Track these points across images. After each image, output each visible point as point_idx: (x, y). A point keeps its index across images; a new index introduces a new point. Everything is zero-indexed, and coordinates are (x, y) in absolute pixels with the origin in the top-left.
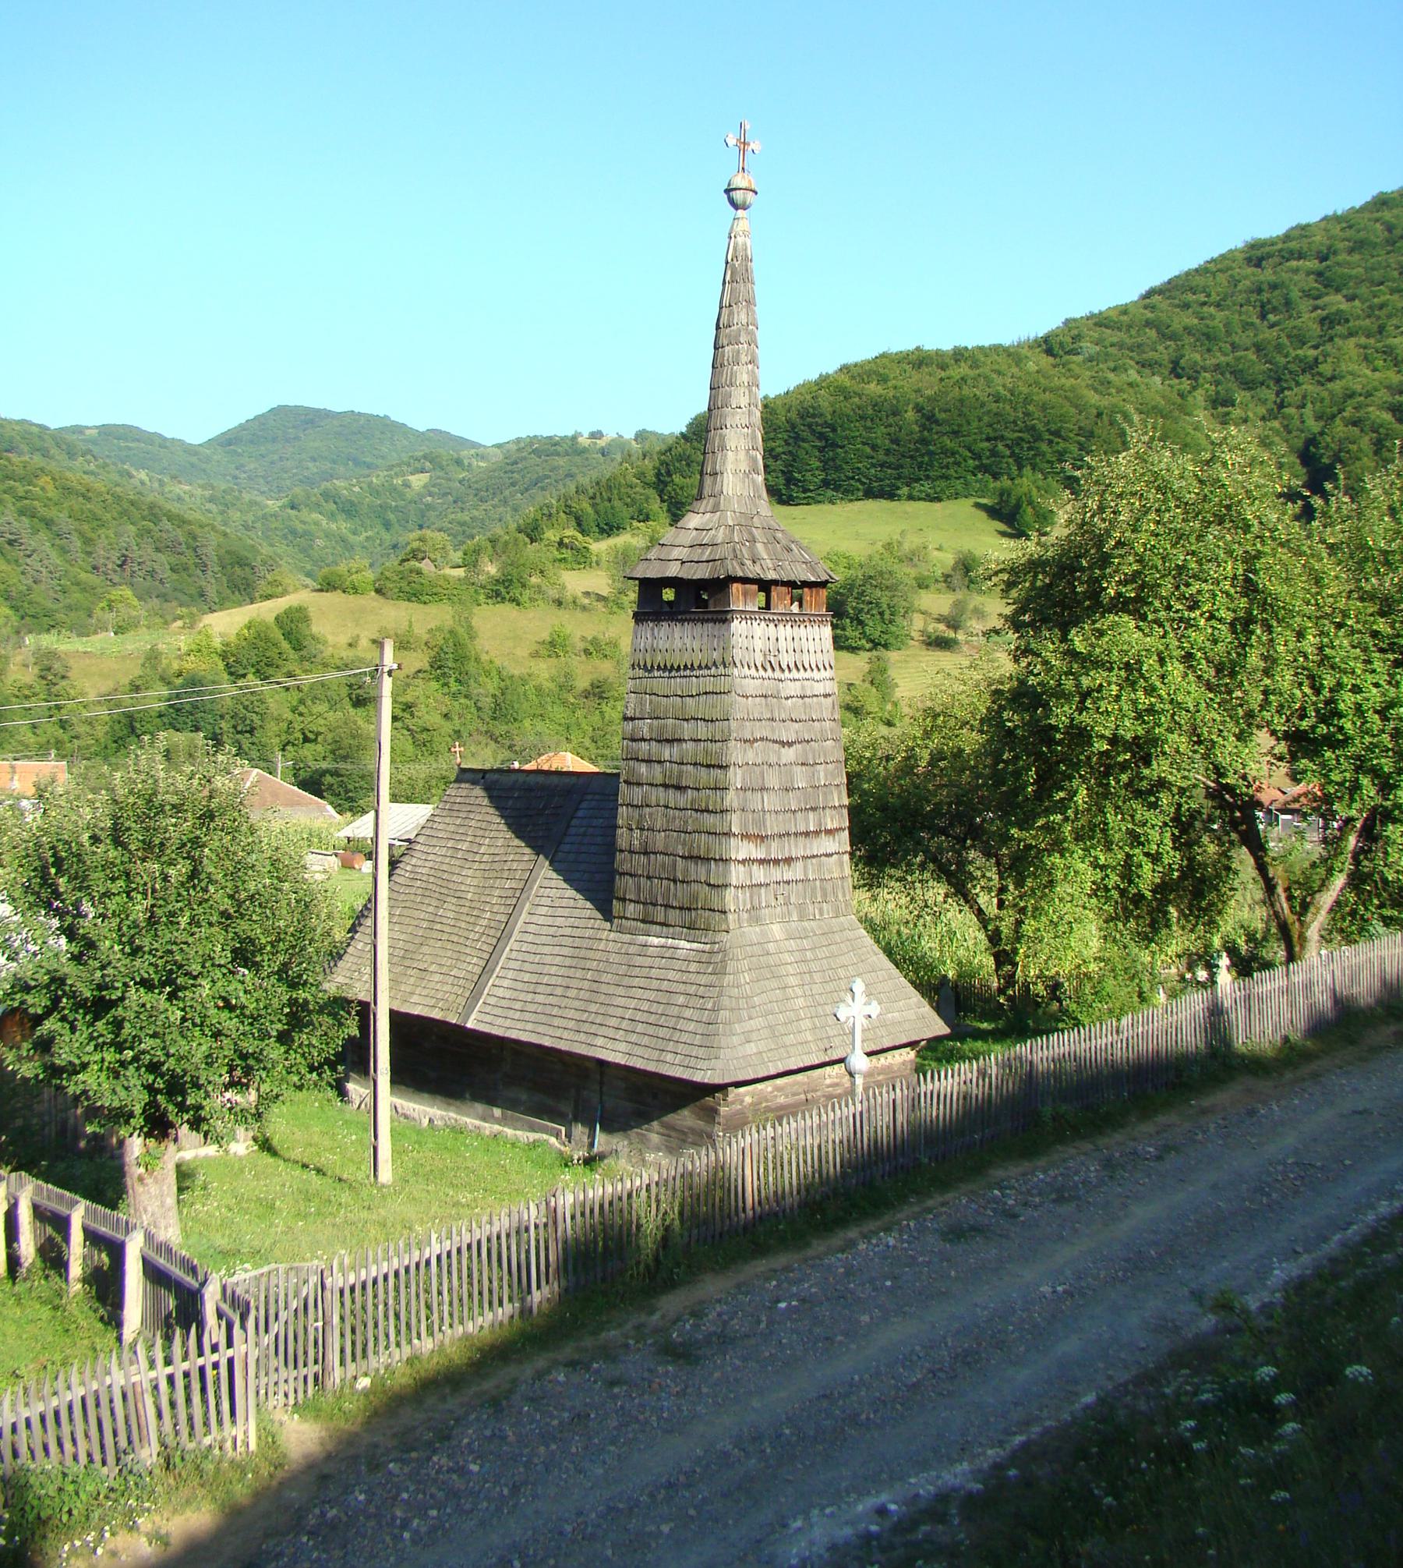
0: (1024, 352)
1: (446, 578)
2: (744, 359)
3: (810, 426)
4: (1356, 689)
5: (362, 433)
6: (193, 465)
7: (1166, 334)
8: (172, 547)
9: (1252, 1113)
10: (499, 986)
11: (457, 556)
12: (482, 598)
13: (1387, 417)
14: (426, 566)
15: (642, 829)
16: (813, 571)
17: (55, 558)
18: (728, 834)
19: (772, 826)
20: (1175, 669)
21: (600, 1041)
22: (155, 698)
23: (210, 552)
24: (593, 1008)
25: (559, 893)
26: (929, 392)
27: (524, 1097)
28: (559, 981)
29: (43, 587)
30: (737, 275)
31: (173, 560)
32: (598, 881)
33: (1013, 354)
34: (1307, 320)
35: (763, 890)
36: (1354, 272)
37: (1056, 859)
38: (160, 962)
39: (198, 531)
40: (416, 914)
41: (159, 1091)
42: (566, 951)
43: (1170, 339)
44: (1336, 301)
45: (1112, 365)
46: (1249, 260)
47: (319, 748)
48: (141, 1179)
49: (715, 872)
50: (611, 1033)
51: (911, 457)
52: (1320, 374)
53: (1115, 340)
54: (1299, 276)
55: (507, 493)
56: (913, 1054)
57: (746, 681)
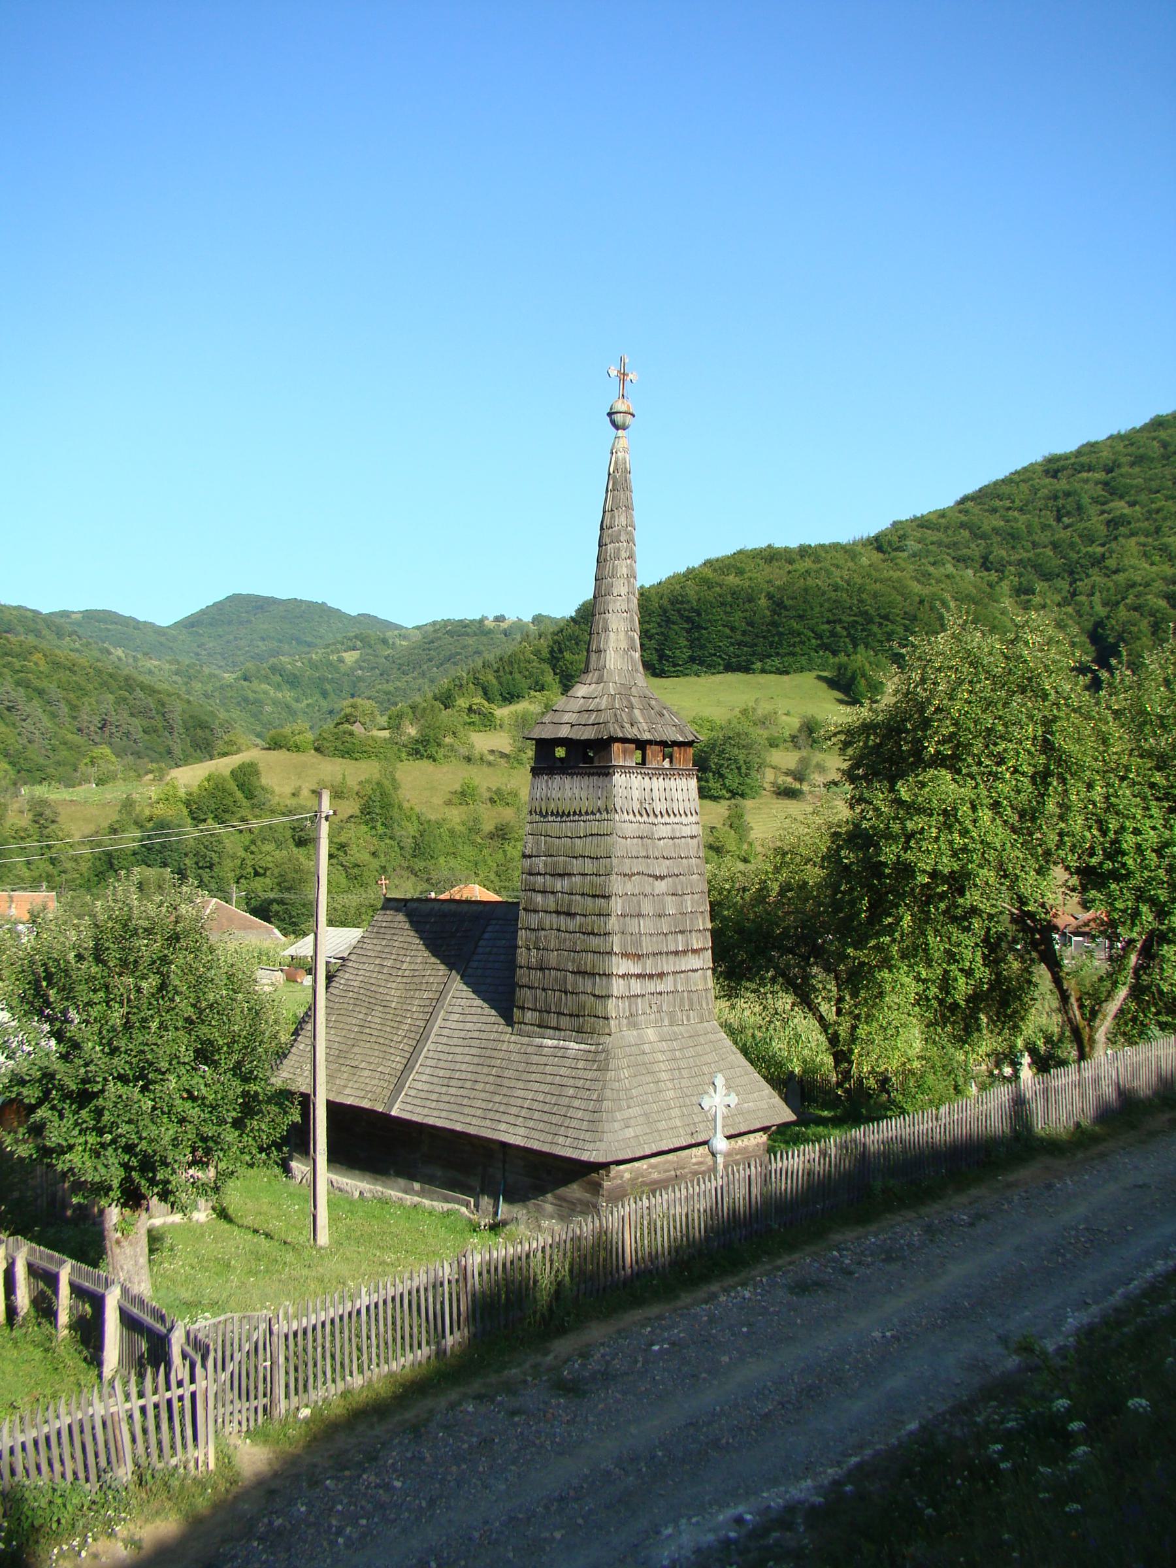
0: (859, 549)
1: (373, 738)
2: (623, 555)
3: (679, 611)
4: (1137, 832)
5: (304, 618)
6: (162, 644)
7: (977, 534)
8: (143, 713)
9: (1049, 1186)
10: (418, 1080)
11: (383, 720)
12: (404, 755)
13: (1163, 603)
14: (357, 728)
15: (539, 949)
16: (682, 732)
17: (47, 722)
18: (610, 953)
19: (647, 946)
20: (985, 815)
21: (503, 1127)
22: (130, 839)
23: (176, 717)
24: (497, 1098)
25: (469, 1003)
26: (778, 583)
27: (439, 1173)
28: (469, 1076)
29: (36, 746)
30: (618, 484)
31: (145, 723)
32: (501, 993)
33: (849, 551)
34: (1096, 522)
35: (640, 1000)
36: (1135, 482)
37: (885, 974)
38: (134, 1060)
39: (166, 699)
40: (349, 1020)
41: (133, 1168)
42: (474, 1051)
43: (981, 538)
44: (1120, 507)
45: (932, 560)
46: (1047, 472)
47: (268, 881)
48: (118, 1242)
49: (599, 985)
50: (512, 1120)
51: (764, 637)
52: (1107, 568)
53: (935, 539)
54: (1089, 486)
55: (425, 667)
56: (765, 1137)
57: (626, 824)
